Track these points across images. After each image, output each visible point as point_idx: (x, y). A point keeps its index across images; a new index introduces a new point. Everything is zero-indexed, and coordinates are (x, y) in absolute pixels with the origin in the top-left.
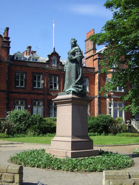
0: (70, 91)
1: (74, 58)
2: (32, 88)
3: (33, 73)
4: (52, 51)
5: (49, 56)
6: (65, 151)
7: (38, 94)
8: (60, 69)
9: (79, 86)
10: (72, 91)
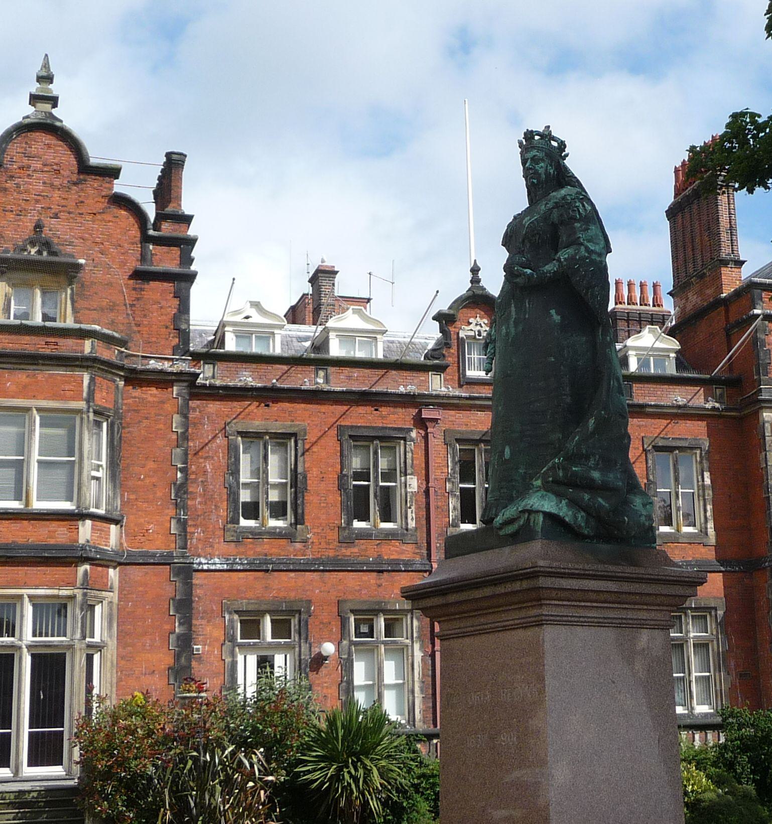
0: (530, 512)
1: (550, 268)
9: (596, 475)
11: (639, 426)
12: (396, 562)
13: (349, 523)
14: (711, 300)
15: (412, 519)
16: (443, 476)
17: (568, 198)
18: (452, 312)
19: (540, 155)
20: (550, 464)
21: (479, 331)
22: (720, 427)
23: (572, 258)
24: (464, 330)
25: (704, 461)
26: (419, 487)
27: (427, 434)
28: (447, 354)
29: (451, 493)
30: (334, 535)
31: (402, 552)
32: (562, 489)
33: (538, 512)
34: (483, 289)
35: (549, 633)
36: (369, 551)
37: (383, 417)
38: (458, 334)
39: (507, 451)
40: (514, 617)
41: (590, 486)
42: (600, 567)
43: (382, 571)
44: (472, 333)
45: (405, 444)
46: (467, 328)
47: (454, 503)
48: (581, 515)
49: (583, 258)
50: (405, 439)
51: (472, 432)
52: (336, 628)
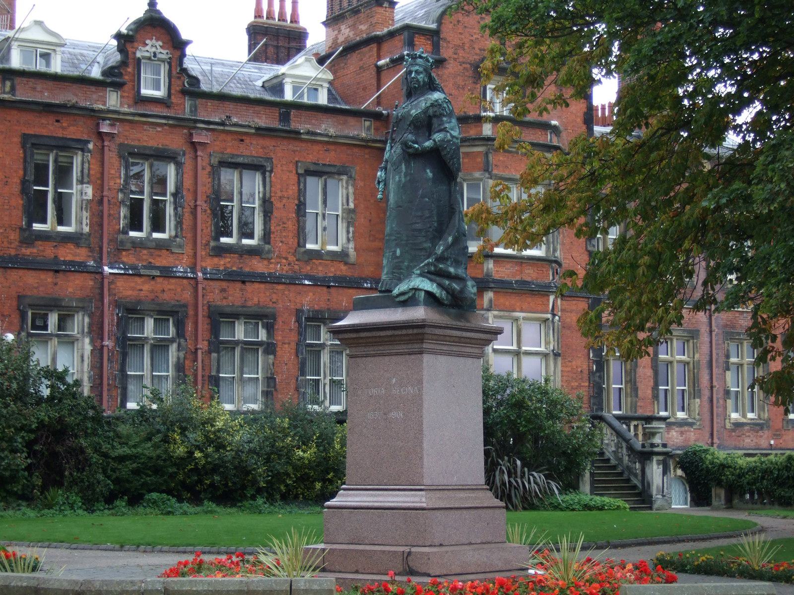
0: (416, 289)
1: (428, 144)
2: (21, 229)
3: (31, 143)
4: (139, 10)
5: (119, 36)
6: (401, 549)
7: (56, 268)
8: (187, 116)
9: (452, 270)
10: (423, 294)
11: (294, 151)
12: (72, 263)
13: (30, 225)
14: (364, 36)
15: (87, 225)
16: (116, 186)
17: (440, 101)
18: (131, 33)
19: (421, 69)
20: (426, 262)
21: (155, 53)
22: (367, 156)
23: (442, 141)
24: (141, 50)
25: (350, 187)
26: (94, 195)
27: (103, 146)
28: (124, 72)
29: (122, 202)
30: (14, 236)
31: (75, 255)
32: (433, 277)
33: (421, 290)
34: (159, 12)
35: (426, 358)
36: (47, 251)
37: (64, 128)
38: (135, 53)
39: (398, 252)
40: (403, 348)
41: (449, 276)
42: (454, 323)
43: (57, 271)
44: (147, 54)
45: (83, 155)
46: (143, 49)
47: (124, 212)
48: (444, 292)
49: (449, 141)
50: (82, 150)
51: (145, 148)
52: (16, 319)
